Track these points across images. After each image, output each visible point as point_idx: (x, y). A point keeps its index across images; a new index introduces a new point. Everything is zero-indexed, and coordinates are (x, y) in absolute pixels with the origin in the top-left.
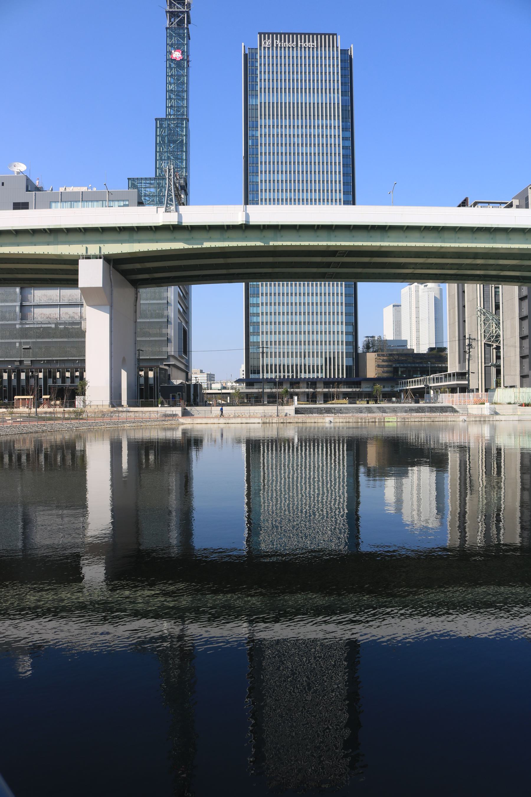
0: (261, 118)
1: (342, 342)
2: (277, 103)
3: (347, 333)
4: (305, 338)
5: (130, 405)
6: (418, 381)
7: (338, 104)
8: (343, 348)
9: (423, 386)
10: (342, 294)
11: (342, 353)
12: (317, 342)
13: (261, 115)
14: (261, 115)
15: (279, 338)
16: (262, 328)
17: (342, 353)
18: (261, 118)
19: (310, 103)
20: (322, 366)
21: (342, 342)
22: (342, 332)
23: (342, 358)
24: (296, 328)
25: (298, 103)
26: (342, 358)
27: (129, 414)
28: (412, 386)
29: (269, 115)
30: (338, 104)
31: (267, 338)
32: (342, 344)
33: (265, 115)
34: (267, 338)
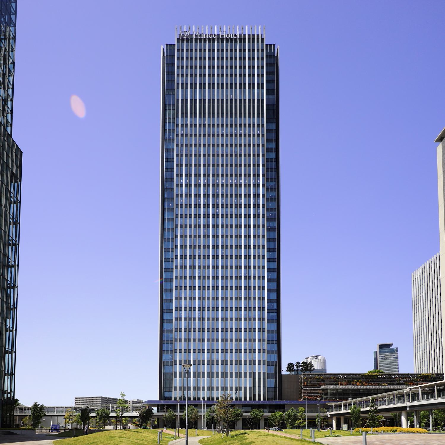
0: (178, 116)
1: (264, 361)
2: (254, 100)
3: (269, 352)
4: (231, 356)
5: (399, 427)
6: (336, 406)
7: (263, 100)
8: (265, 369)
9: (349, 411)
10: (264, 308)
11: (264, 373)
12: (255, 361)
13: (178, 113)
14: (178, 113)
15: (255, 357)
16: (176, 346)
17: (264, 373)
18: (178, 116)
19: (200, 100)
20: (250, 388)
21: (264, 361)
22: (264, 350)
23: (264, 379)
24: (231, 346)
25: (187, 100)
26: (264, 379)
27: (275, 438)
28: (332, 411)
29: (191, 113)
30: (263, 100)
31: (190, 356)
32: (264, 364)
33: (209, 113)
34: (190, 356)
